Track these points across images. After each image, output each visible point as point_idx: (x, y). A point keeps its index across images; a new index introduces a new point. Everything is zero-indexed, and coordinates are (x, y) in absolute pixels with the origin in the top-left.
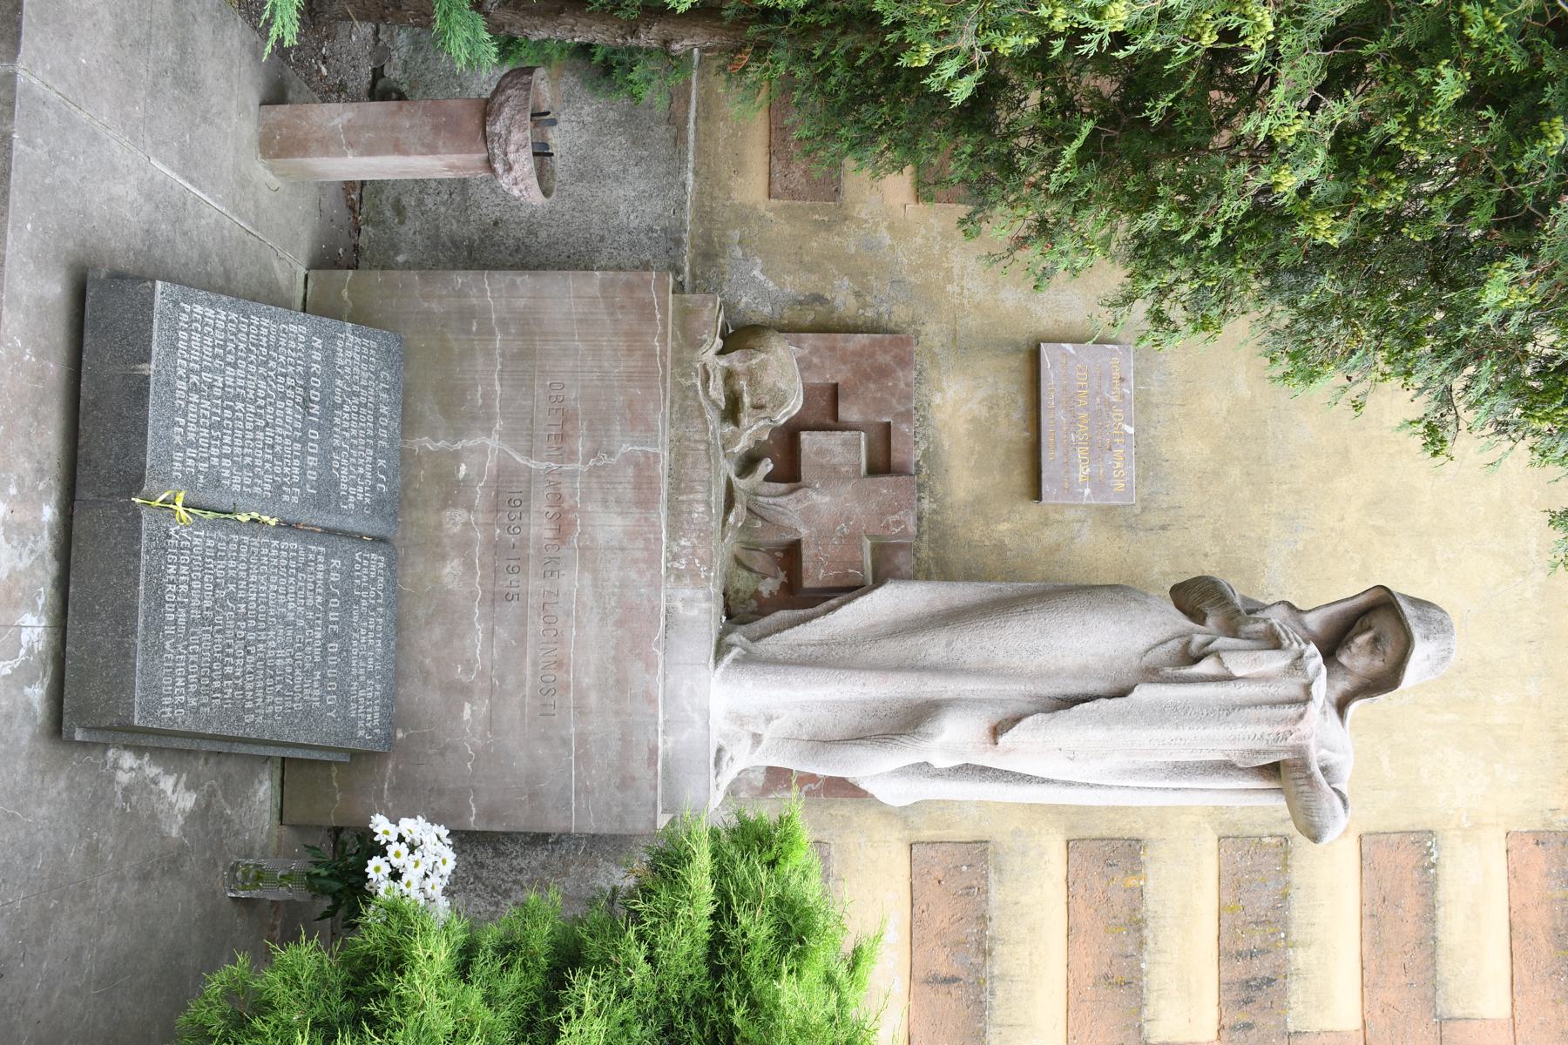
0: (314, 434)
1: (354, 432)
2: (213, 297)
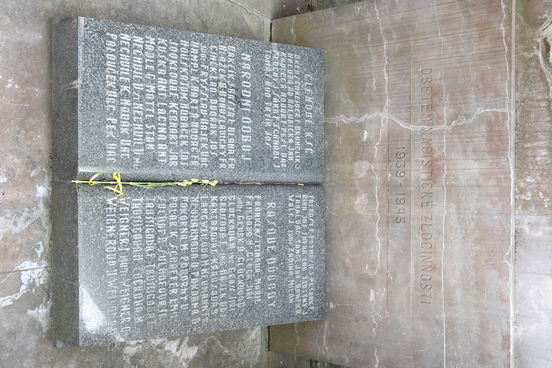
2: (141, 28)
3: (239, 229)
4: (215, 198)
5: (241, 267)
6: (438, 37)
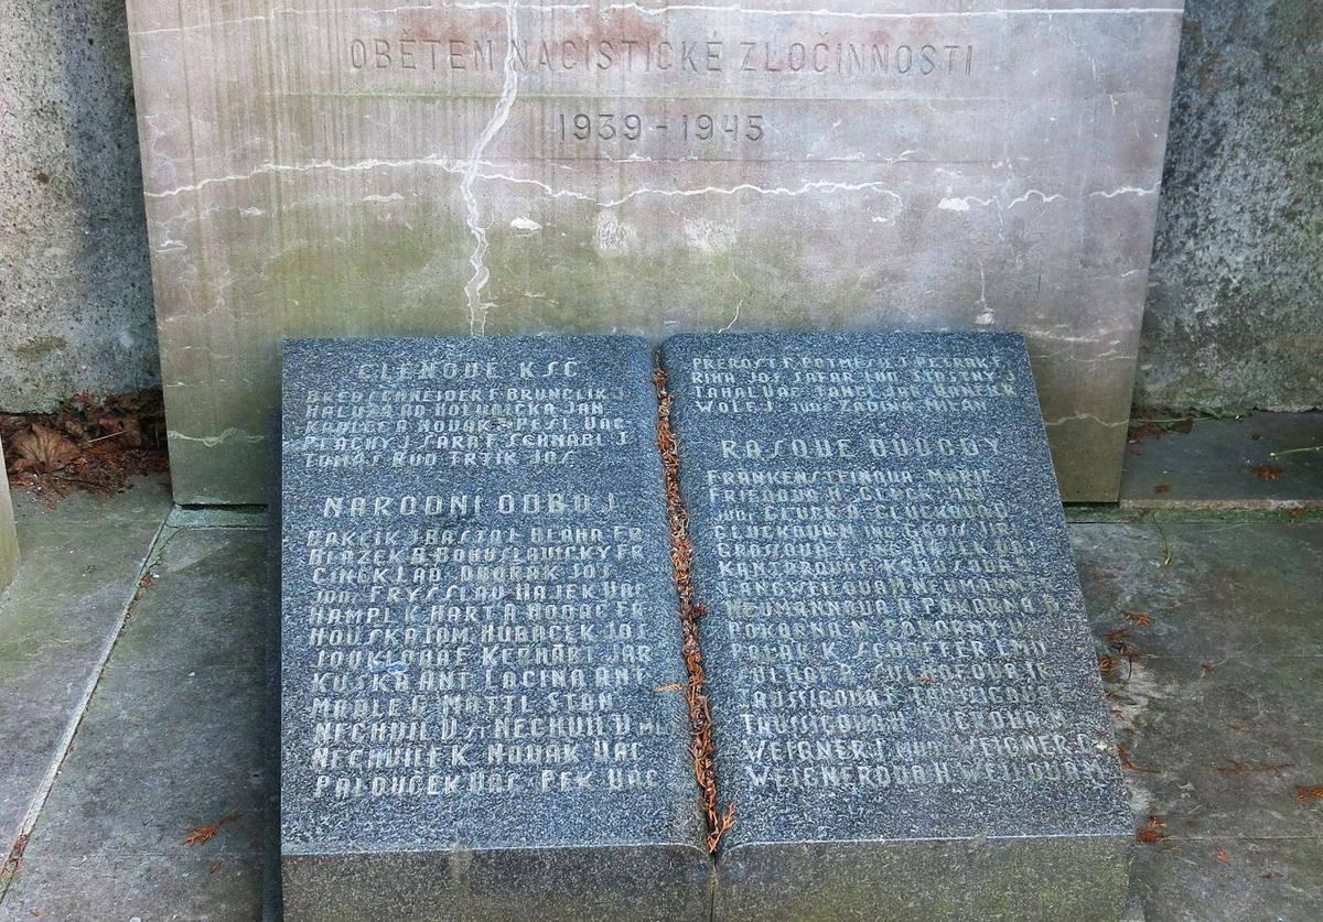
0: (505, 503)
1: (483, 426)
2: (289, 728)
3: (800, 516)
4: (724, 568)
5: (900, 511)
6: (267, 22)
